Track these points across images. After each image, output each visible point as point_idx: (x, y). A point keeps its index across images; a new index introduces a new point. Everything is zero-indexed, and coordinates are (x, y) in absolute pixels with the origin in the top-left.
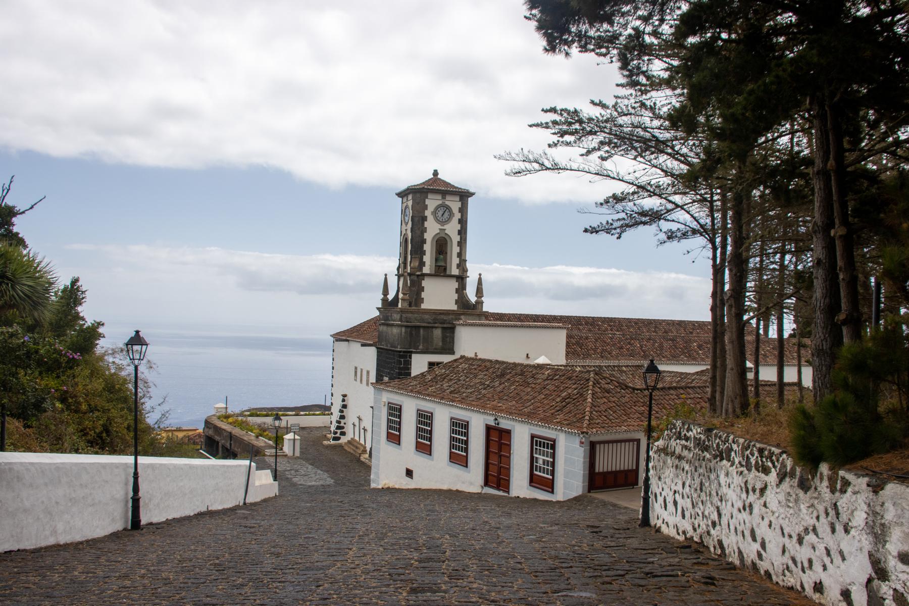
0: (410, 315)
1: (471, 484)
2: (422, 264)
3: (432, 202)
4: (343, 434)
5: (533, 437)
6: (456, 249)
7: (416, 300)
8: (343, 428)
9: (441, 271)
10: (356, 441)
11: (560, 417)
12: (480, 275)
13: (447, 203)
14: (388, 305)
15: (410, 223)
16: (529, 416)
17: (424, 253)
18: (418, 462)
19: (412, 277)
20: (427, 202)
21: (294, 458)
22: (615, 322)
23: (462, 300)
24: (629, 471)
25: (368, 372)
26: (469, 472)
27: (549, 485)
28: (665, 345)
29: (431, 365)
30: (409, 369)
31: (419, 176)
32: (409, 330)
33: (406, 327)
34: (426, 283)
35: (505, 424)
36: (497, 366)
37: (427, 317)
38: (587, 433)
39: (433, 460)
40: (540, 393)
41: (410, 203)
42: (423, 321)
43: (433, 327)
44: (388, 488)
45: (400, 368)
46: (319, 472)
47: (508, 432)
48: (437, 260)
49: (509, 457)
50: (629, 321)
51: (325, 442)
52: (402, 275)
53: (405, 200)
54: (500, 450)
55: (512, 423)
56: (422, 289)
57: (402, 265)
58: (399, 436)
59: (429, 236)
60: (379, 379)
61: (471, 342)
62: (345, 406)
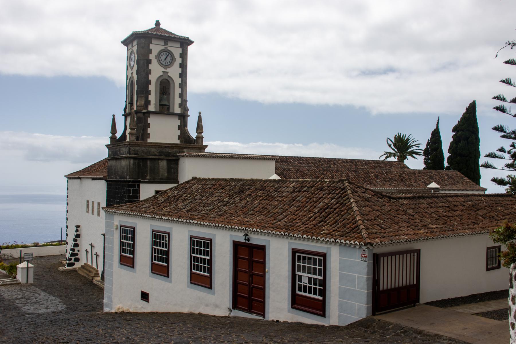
1: (217, 306)
2: (148, 103)
3: (156, 47)
4: (77, 260)
5: (294, 252)
6: (178, 91)
7: (142, 135)
8: (77, 254)
9: (164, 110)
10: (88, 266)
11: (326, 229)
12: (200, 113)
13: (169, 48)
14: (115, 143)
15: (136, 66)
16: (288, 229)
17: (149, 93)
18: (155, 285)
19: (139, 115)
20: (151, 46)
21: (28, 285)
22: (303, 160)
23: (184, 136)
24: (410, 286)
26: (214, 294)
27: (319, 308)
28: (350, 175)
29: (157, 192)
31: (145, 25)
32: (137, 161)
33: (134, 159)
34: (151, 120)
35: (257, 239)
36: (233, 184)
37: (153, 150)
38: (371, 244)
39: (171, 282)
40: (290, 205)
41: (135, 49)
43: (159, 159)
44: (122, 313)
46: (52, 297)
47: (262, 249)
49: (264, 276)
50: (314, 159)
51: (61, 268)
52: (129, 114)
53: (130, 46)
54: (251, 268)
55: (266, 238)
56: (148, 125)
57: (129, 106)
58: (133, 259)
59: (153, 78)
60: (109, 203)
62: (78, 236)
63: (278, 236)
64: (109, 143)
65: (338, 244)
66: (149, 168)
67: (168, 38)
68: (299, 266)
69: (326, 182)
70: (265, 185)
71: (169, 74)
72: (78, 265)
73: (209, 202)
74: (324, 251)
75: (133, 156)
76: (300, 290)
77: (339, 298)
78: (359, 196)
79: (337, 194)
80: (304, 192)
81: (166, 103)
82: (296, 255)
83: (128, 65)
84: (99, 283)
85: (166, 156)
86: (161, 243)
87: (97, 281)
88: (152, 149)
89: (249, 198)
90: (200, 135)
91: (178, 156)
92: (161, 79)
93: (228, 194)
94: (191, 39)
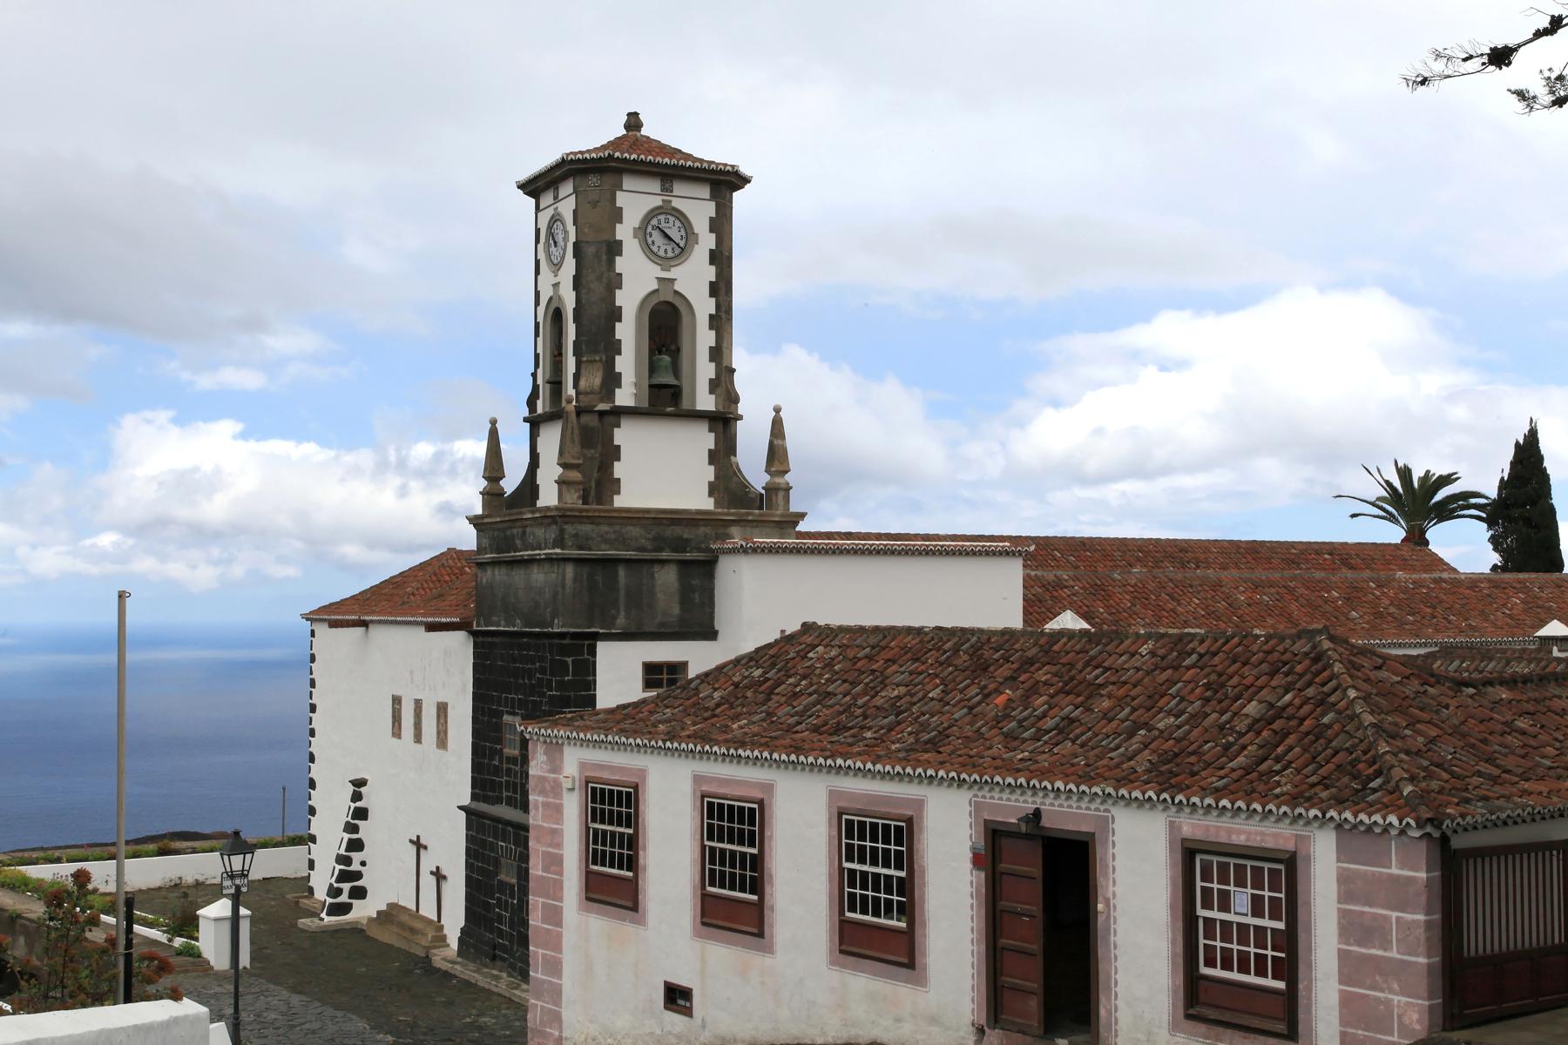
0: (586, 528)
4: (359, 893)
6: (705, 338)
7: (598, 484)
8: (358, 876)
9: (666, 401)
12: (777, 410)
13: (676, 203)
14: (505, 512)
16: (1170, 777)
17: (615, 348)
18: (711, 965)
19: (585, 419)
20: (621, 199)
23: (727, 483)
25: (442, 709)
30: (591, 685)
31: (595, 132)
32: (585, 570)
33: (578, 561)
34: (626, 435)
35: (1065, 811)
41: (567, 207)
42: (623, 542)
45: (562, 685)
46: (330, 1011)
48: (653, 369)
53: (547, 199)
56: (615, 453)
59: (629, 299)
61: (760, 603)
63: (1135, 805)
64: (479, 511)
65: (1332, 825)
66: (622, 592)
67: (672, 169)
68: (1207, 892)
69: (1258, 637)
70: (1056, 648)
71: (677, 288)
72: (363, 911)
73: (878, 701)
74: (1290, 846)
75: (575, 553)
76: (1210, 963)
77: (1340, 983)
78: (1368, 680)
79: (1301, 676)
80: (1188, 668)
81: (670, 380)
82: (1190, 856)
83: (542, 256)
84: (458, 967)
85: (675, 550)
86: (734, 836)
87: (445, 959)
88: (630, 528)
89: (1014, 690)
90: (778, 480)
91: (712, 551)
92: (654, 301)
93: (937, 676)
94: (745, 170)
